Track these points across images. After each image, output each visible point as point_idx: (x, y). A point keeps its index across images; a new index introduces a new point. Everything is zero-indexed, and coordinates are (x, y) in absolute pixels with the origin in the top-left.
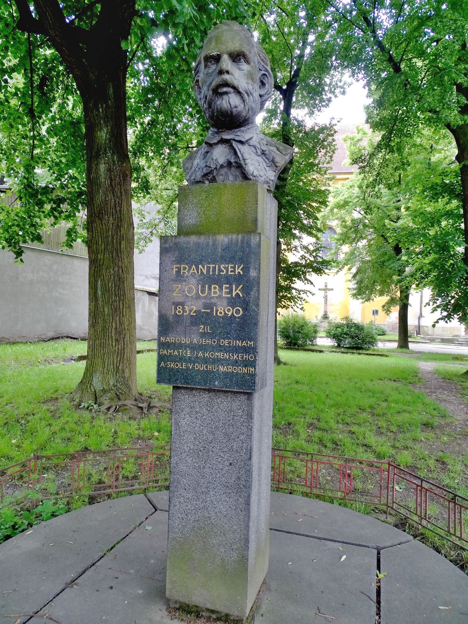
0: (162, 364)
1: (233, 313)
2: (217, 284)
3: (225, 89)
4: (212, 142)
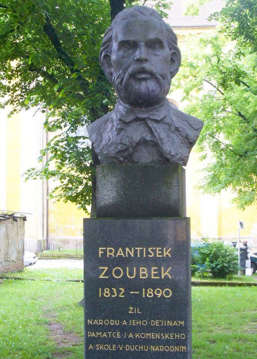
0: (91, 347)
1: (162, 294)
2: (145, 267)
3: (143, 76)
4: (127, 121)
